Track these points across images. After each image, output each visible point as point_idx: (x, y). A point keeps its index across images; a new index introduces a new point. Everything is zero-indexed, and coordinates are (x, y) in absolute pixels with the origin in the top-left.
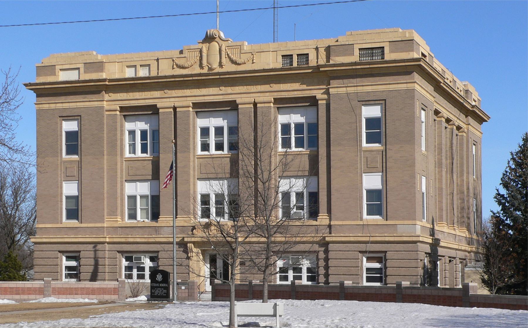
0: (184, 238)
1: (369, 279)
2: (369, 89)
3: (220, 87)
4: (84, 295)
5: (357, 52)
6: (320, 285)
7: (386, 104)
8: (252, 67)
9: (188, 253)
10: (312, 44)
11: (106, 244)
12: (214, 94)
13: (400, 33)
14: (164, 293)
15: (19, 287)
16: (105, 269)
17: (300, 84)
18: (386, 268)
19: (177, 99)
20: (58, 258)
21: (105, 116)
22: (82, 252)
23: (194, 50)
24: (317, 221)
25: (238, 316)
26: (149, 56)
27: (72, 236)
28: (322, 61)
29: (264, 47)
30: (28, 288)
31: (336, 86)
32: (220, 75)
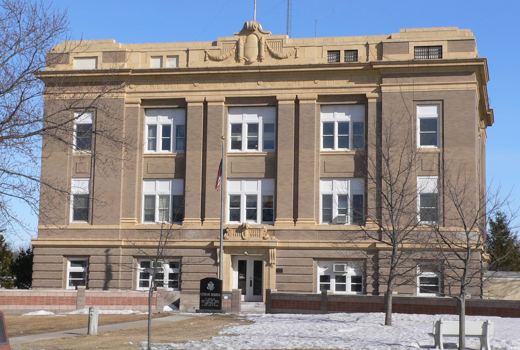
0: (213, 242)
1: (421, 291)
2: (426, 88)
3: (258, 82)
4: (120, 305)
5: (412, 50)
6: (367, 295)
7: (444, 105)
8: (294, 62)
9: (217, 259)
10: (362, 40)
11: (121, 248)
12: (252, 88)
13: (458, 33)
14: (216, 304)
15: (50, 297)
16: (119, 275)
17: (348, 82)
18: (88, 272)
19: (208, 93)
20: (62, 263)
21: (125, 109)
22: (91, 256)
23: (230, 42)
24: (273, 225)
25: (444, 335)
26: (178, 47)
27: (81, 239)
28: (373, 57)
29: (307, 41)
30: (59, 297)
31: (389, 84)
32: (260, 69)
